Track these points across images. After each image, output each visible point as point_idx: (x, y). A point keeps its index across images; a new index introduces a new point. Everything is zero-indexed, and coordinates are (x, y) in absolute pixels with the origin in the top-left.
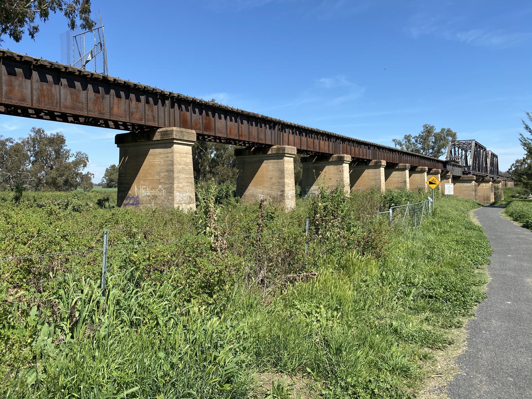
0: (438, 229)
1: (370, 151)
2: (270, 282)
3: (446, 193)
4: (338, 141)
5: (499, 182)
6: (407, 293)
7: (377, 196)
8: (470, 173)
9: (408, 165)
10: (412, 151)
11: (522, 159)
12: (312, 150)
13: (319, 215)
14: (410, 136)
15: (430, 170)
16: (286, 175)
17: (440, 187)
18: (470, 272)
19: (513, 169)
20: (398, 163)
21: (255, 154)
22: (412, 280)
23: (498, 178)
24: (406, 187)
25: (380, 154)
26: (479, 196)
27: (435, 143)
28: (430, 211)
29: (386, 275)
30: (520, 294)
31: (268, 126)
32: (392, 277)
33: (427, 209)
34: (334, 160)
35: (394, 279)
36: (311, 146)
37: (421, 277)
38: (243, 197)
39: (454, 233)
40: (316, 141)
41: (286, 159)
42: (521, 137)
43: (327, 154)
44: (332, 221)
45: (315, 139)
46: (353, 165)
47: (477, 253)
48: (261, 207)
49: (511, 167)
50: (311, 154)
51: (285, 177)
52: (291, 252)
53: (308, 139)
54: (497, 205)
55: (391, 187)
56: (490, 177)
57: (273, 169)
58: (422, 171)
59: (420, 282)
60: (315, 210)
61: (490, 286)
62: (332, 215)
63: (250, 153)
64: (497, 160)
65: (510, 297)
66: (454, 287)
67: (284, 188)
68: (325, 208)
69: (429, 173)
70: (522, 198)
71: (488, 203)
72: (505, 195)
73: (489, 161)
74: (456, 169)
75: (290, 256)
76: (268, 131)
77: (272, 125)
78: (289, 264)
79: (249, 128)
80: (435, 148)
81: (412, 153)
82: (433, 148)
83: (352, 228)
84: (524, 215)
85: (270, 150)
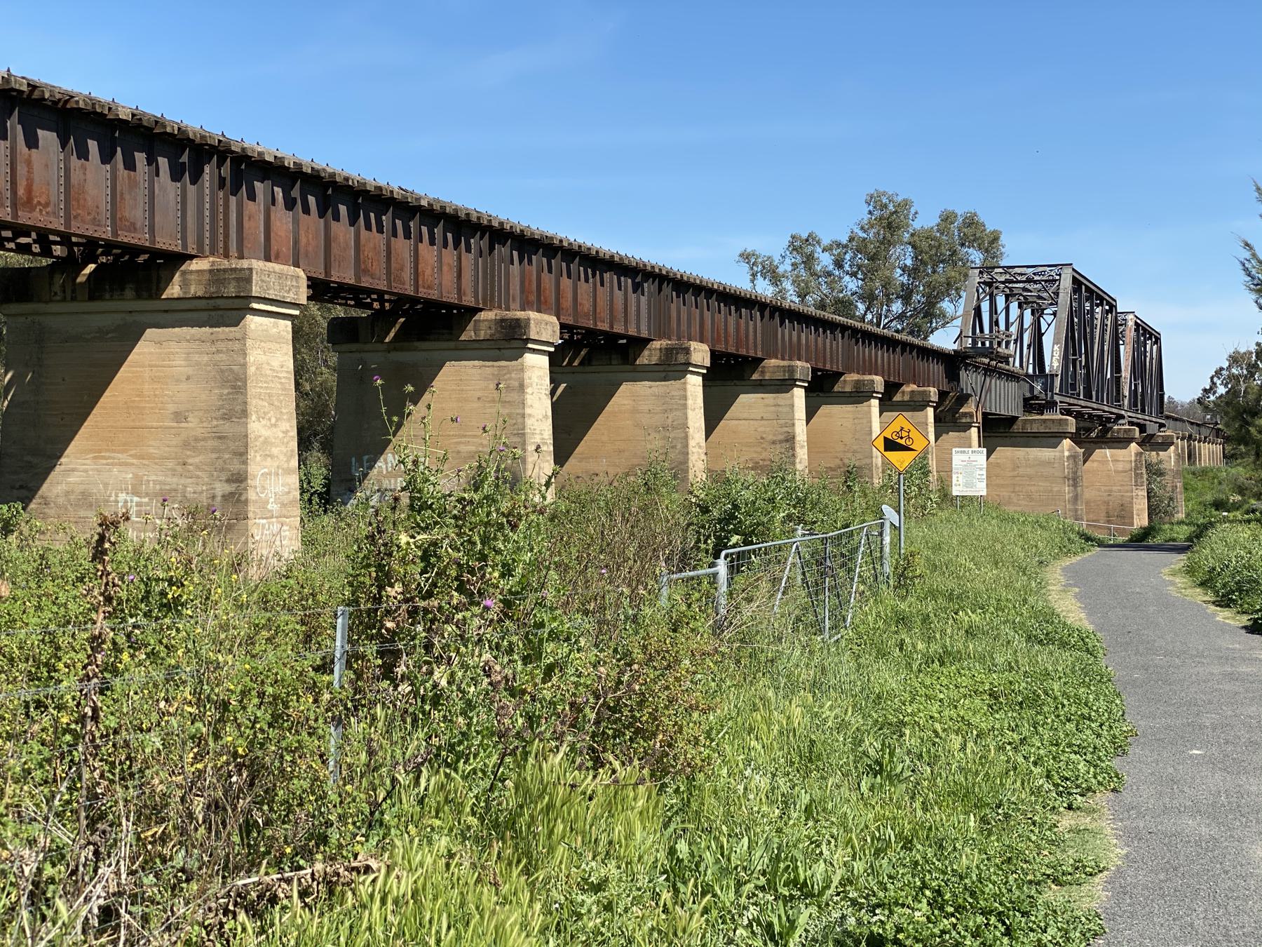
0: (920, 646)
1: (643, 299)
2: (145, 919)
3: (956, 491)
4: (502, 250)
5: (1166, 444)
6: (777, 929)
7: (669, 505)
8: (1051, 405)
9: (802, 367)
10: (822, 306)
12: (382, 285)
13: (398, 588)
14: (811, 240)
15: (892, 388)
16: (254, 404)
17: (933, 464)
18: (1041, 825)
19: (1221, 390)
20: (760, 355)
21: (100, 298)
22: (801, 871)
23: (1162, 425)
24: (794, 464)
25: (684, 316)
26: (1087, 503)
27: (913, 272)
28: (888, 569)
29: (692, 854)
30: (1231, 909)
31: (163, 162)
32: (717, 861)
33: (876, 559)
34: (482, 336)
35: (724, 872)
36: (379, 268)
37: (841, 855)
38: (32, 506)
39: (981, 660)
40: (402, 246)
41: (253, 323)
42: (1247, 255)
43: (450, 306)
44: (459, 616)
45: (395, 235)
46: (570, 363)
47: (1070, 745)
48: (105, 552)
49: (1214, 383)
50: (376, 305)
51: (251, 408)
52: (255, 769)
53: (363, 232)
54: (1158, 540)
55: (729, 465)
56: (1131, 423)
57: (190, 371)
58: (859, 395)
59: (836, 880)
60: (380, 567)
61: (1120, 889)
62: (460, 589)
63: (73, 293)
64: (1160, 350)
65: (1191, 925)
66: (973, 894)
67: (245, 463)
68: (428, 554)
69: (887, 403)
70: (1254, 511)
71: (1122, 532)
72: (1188, 500)
73: (1125, 353)
74: (996, 384)
75: (252, 785)
76: (167, 188)
77: (185, 158)
78: (248, 827)
79: (67, 170)
80: (916, 297)
81: (820, 313)
82: (906, 297)
83: (549, 647)
84: (1255, 581)
85: (177, 277)
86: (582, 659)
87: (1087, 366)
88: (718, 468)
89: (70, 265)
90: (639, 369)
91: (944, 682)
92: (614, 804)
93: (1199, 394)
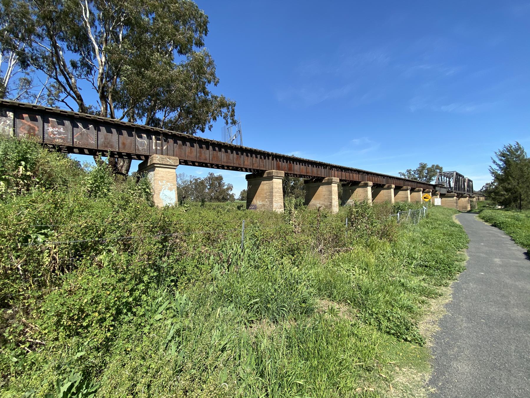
3: (435, 204)
5: (474, 197)
7: (389, 206)
8: (452, 192)
10: (412, 179)
11: (491, 182)
14: (410, 170)
15: (424, 190)
16: (333, 194)
17: (431, 200)
19: (484, 189)
28: (425, 215)
33: (423, 214)
36: (348, 177)
37: (419, 254)
39: (442, 228)
40: (351, 174)
54: (473, 212)
58: (419, 191)
63: (313, 182)
68: (357, 212)
69: (423, 192)
73: (466, 184)
76: (323, 170)
82: (426, 177)
86: (378, 226)
87: (459, 186)
88: (397, 201)
89: (312, 179)
90: (150, 167)
91: (435, 232)
92: (384, 244)
93: (480, 190)
